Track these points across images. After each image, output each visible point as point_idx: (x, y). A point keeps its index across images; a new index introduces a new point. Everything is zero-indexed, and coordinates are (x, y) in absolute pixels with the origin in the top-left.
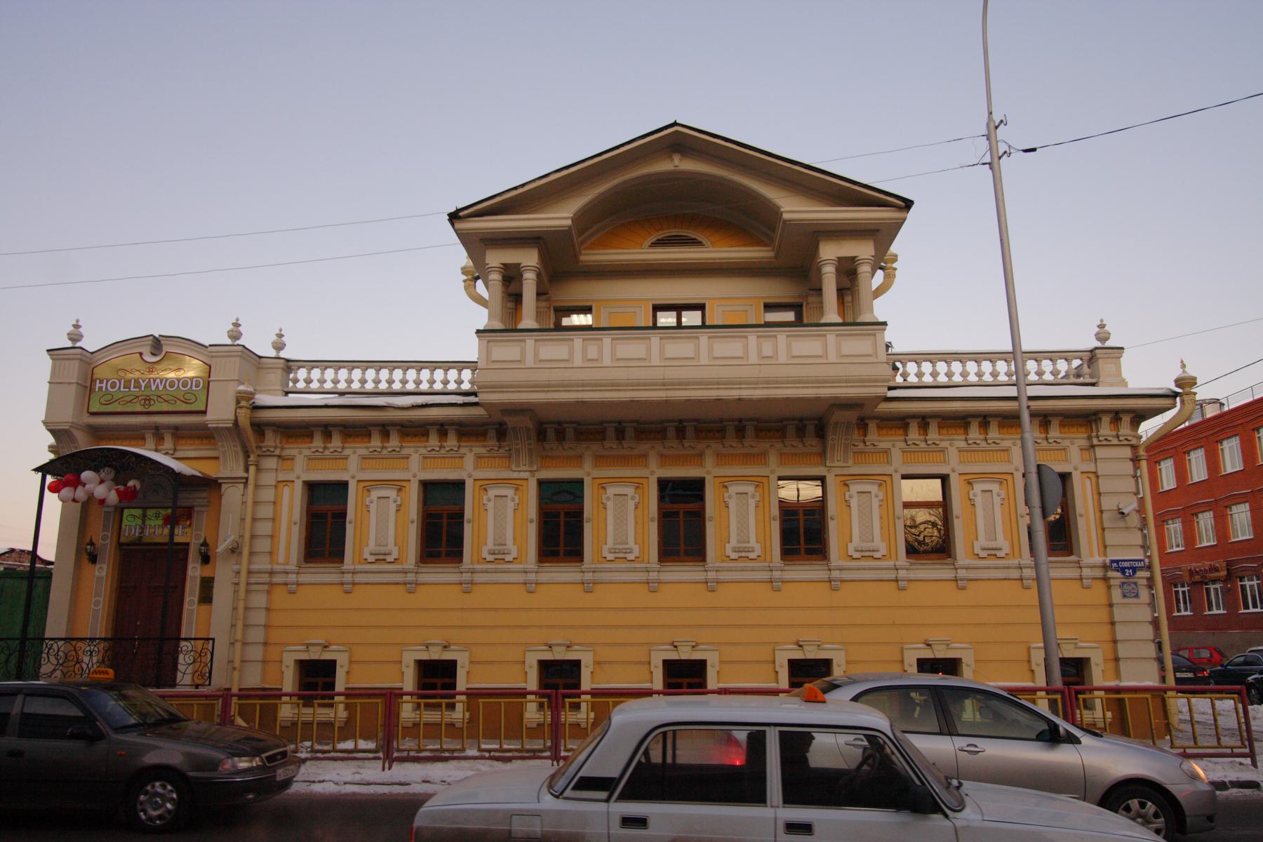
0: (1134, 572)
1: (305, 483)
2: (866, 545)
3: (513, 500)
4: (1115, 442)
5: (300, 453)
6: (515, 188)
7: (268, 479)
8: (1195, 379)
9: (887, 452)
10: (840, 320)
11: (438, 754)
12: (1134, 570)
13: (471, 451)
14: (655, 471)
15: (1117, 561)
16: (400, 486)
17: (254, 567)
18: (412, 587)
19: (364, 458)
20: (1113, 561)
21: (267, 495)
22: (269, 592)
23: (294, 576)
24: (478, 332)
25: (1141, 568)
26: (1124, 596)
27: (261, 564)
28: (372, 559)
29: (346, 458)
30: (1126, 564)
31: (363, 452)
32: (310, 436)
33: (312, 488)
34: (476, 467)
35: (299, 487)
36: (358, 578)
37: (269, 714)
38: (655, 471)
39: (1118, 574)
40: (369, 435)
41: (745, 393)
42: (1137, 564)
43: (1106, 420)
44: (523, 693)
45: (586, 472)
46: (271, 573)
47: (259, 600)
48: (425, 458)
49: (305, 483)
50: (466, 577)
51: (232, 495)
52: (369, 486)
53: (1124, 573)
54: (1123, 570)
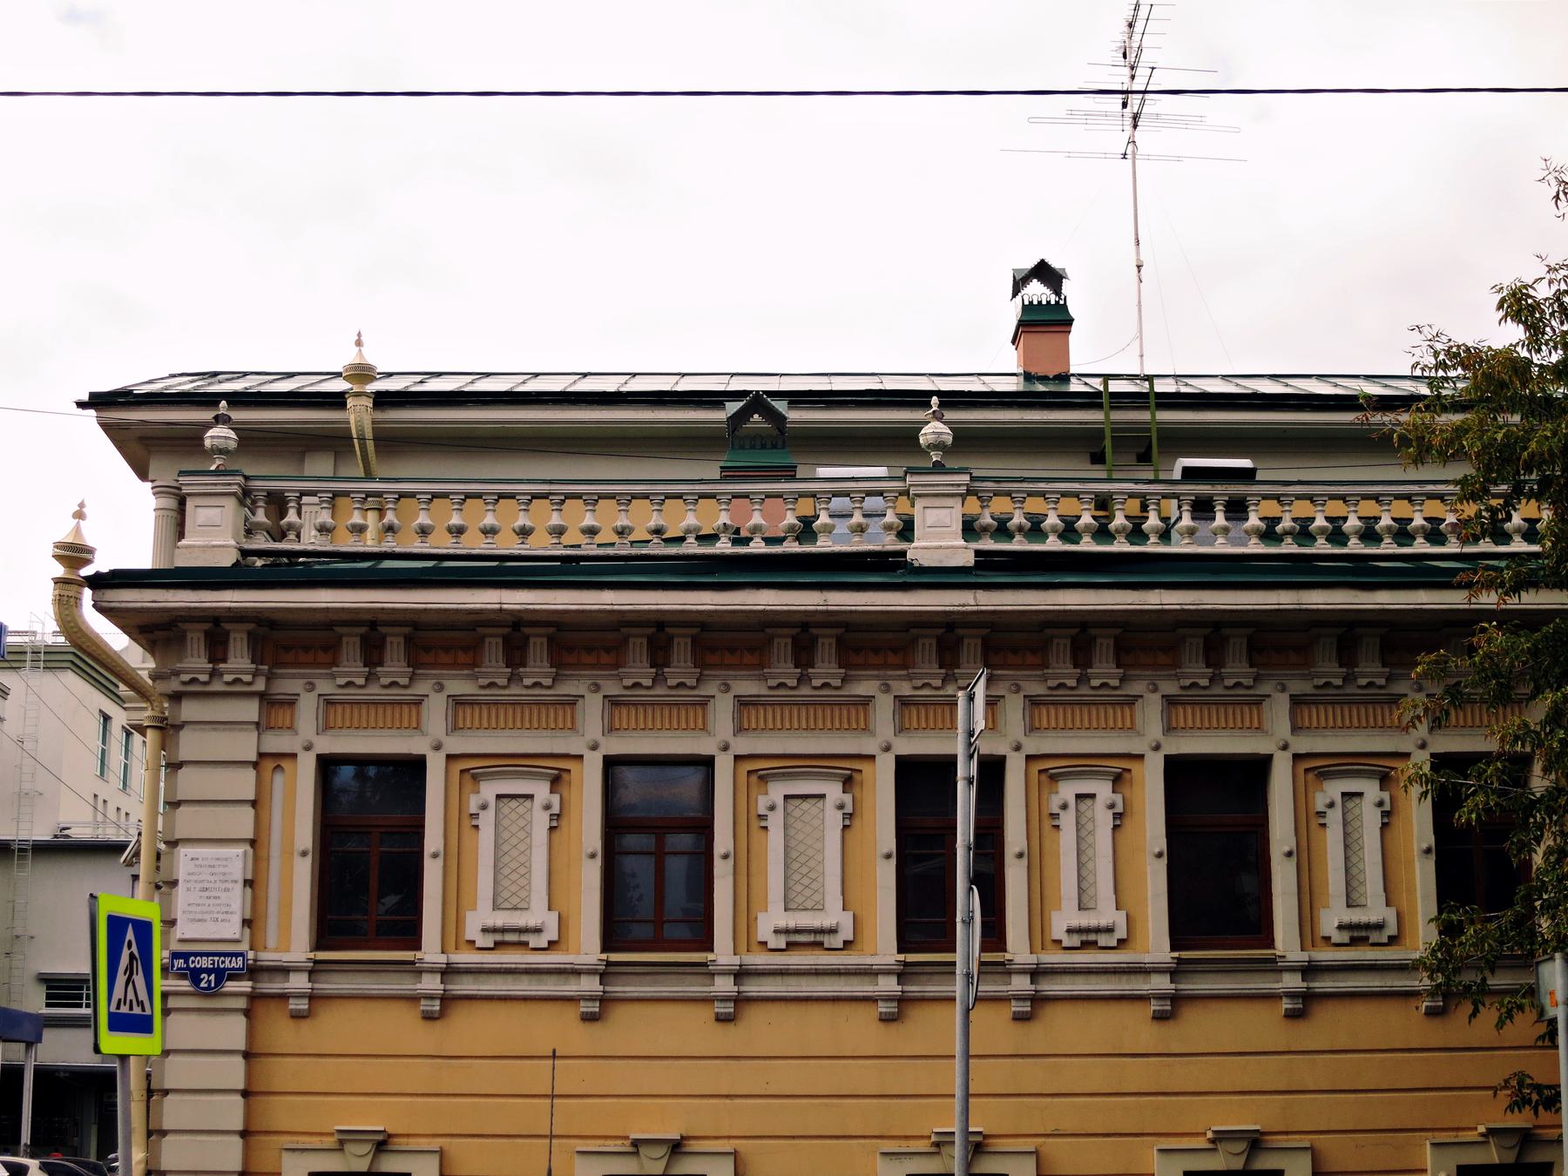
0: (219, 982)
2: (501, 919)
3: (547, 807)
5: (311, 687)
8: (91, 551)
9: (866, 702)
12: (221, 975)
13: (887, 689)
14: (885, 741)
15: (185, 956)
16: (1382, 768)
22: (247, 1013)
25: (234, 976)
29: (418, 703)
30: (205, 963)
31: (1170, 688)
33: (907, 768)
34: (455, 728)
39: (185, 985)
40: (181, 639)
42: (228, 963)
45: (430, 734)
48: (329, 703)
49: (900, 761)
52: (470, 768)
53: (196, 981)
54: (194, 975)
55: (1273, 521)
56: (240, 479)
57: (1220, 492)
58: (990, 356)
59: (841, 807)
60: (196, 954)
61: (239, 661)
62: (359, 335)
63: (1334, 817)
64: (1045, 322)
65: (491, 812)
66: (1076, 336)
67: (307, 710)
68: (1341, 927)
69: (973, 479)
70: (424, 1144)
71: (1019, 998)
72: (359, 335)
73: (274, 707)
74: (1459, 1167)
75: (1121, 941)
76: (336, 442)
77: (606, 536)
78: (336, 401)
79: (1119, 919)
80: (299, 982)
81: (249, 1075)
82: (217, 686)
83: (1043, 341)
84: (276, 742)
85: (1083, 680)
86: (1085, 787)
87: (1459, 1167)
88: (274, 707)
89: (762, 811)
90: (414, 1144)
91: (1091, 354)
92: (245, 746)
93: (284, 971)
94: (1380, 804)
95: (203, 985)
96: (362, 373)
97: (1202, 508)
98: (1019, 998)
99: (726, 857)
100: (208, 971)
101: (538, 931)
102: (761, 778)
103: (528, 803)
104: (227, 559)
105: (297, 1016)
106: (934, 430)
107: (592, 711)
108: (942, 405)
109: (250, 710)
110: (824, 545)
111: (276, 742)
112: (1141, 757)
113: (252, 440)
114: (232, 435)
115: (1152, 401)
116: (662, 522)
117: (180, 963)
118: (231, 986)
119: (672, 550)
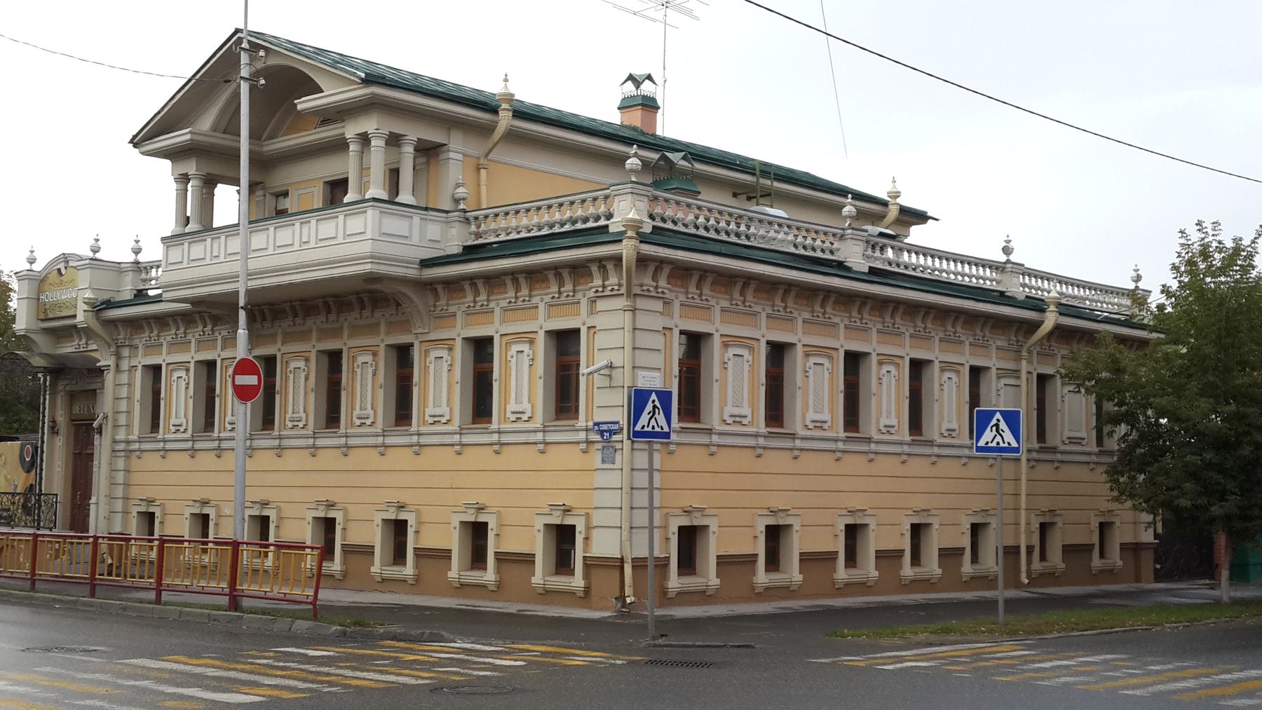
1: (548, 333)
4: (654, 294)
6: (159, 112)
7: (125, 365)
10: (386, 198)
11: (1179, 674)
17: (118, 438)
18: (193, 452)
19: (505, 310)
20: (595, 424)
21: (124, 378)
23: (381, 439)
24: (163, 239)
26: (603, 461)
27: (121, 436)
28: (431, 420)
30: (605, 427)
32: (545, 280)
34: (503, 321)
35: (140, 367)
36: (505, 439)
37: (122, 554)
38: (386, 339)
40: (462, 289)
41: (336, 272)
43: (594, 269)
44: (302, 547)
46: (128, 442)
47: (121, 464)
50: (495, 437)
51: (109, 378)
54: (602, 433)
63: (291, 376)
64: (95, 250)
80: (136, 446)
104: (456, 250)
118: (615, 438)
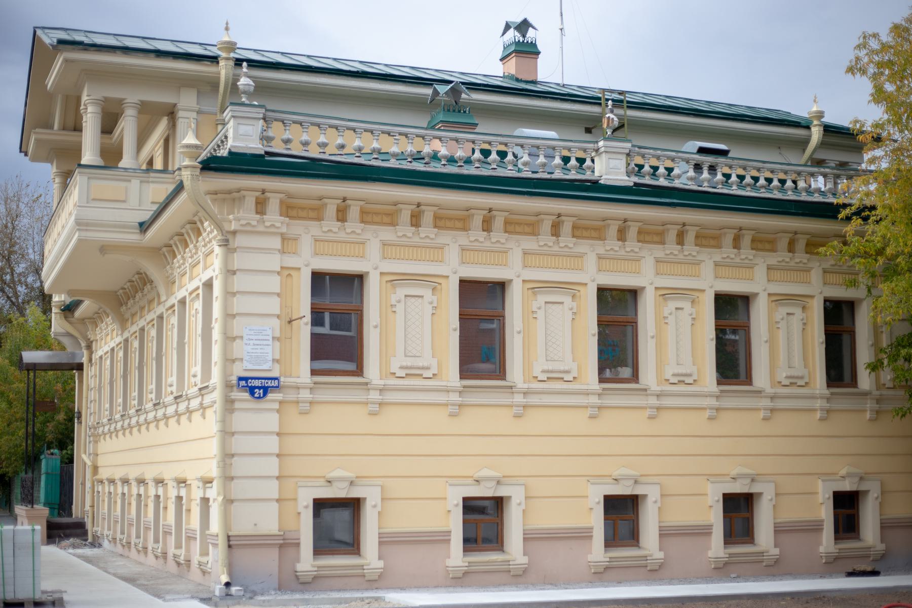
0: (265, 394)
2: (409, 362)
9: (581, 256)
15: (246, 379)
30: (257, 383)
42: (270, 383)
48: (316, 240)
53: (252, 393)
54: (252, 390)
55: (641, 167)
56: (263, 111)
57: (708, 159)
58: (486, 61)
59: (431, 303)
60: (252, 378)
61: (273, 216)
62: (227, 24)
63: (782, 325)
64: (526, 51)
65: (403, 303)
66: (541, 59)
67: (306, 245)
68: (787, 377)
69: (633, 146)
70: (655, 479)
71: (651, 408)
72: (227, 24)
73: (288, 243)
74: (724, 494)
75: (806, 383)
76: (211, 85)
77: (331, 149)
78: (214, 59)
79: (434, 363)
81: (281, 446)
82: (261, 228)
83: (526, 61)
84: (291, 261)
85: (682, 251)
86: (679, 304)
87: (724, 494)
88: (288, 243)
89: (394, 303)
90: (649, 479)
91: (548, 71)
92: (274, 262)
93: (298, 388)
94: (802, 320)
95: (256, 395)
96: (231, 46)
97: (698, 167)
98: (651, 408)
99: (376, 327)
100: (259, 388)
101: (428, 368)
102: (533, 293)
103: (420, 300)
105: (303, 413)
106: (612, 117)
107: (591, 261)
108: (613, 106)
109: (276, 243)
110: (677, 184)
111: (291, 261)
112: (704, 291)
113: (262, 89)
114: (252, 83)
115: (625, 104)
116: (290, 137)
117: (243, 383)
119: (548, 176)
